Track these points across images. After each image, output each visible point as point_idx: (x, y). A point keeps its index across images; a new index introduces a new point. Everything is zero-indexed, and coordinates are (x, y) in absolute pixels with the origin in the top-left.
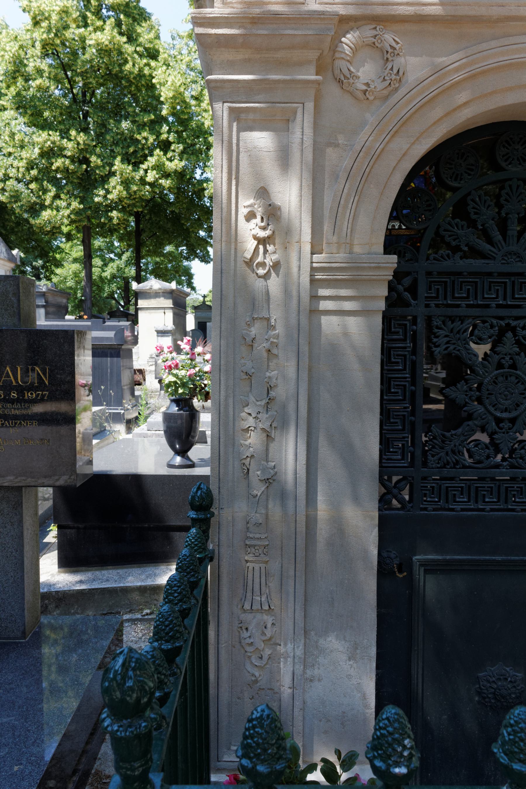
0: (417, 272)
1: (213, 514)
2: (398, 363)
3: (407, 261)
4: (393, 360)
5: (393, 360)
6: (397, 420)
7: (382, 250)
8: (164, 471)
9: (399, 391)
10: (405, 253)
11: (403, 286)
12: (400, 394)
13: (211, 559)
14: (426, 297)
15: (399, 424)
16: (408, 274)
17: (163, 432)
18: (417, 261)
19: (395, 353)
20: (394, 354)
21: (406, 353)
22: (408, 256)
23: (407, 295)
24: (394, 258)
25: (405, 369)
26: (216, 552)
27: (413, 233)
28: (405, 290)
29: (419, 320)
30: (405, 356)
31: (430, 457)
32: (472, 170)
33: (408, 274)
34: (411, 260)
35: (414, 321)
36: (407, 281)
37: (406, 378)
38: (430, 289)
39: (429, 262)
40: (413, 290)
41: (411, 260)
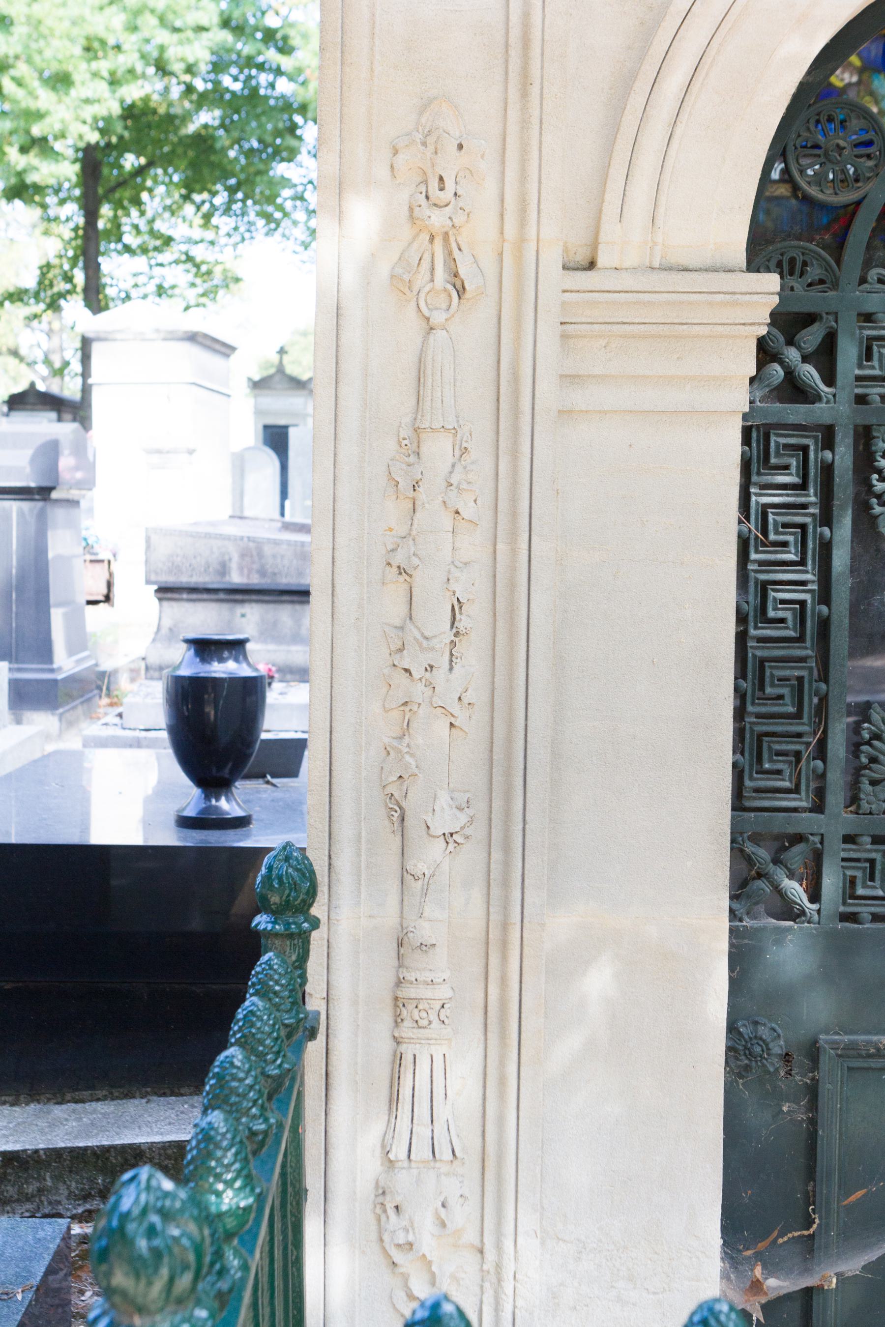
0: (836, 314)
1: (315, 924)
2: (785, 544)
3: (810, 285)
4: (771, 614)
5: (771, 614)
6: (780, 766)
7: (740, 256)
8: (168, 837)
9: (790, 538)
10: (805, 264)
11: (799, 348)
12: (790, 623)
13: (312, 1034)
14: (859, 378)
15: (788, 700)
16: (810, 319)
17: (164, 735)
18: (835, 286)
19: (778, 518)
20: (772, 676)
21: (808, 520)
22: (814, 272)
23: (810, 373)
24: (771, 281)
25: (802, 562)
26: (323, 1017)
27: (185, 1162)
28: (805, 359)
29: (838, 437)
30: (803, 527)
31: (866, 786)
32: (792, 261)
33: (810, 319)
34: (822, 282)
35: (828, 439)
36: (812, 337)
37: (803, 583)
38: (869, 356)
39: (866, 286)
40: (825, 357)
41: (822, 282)
